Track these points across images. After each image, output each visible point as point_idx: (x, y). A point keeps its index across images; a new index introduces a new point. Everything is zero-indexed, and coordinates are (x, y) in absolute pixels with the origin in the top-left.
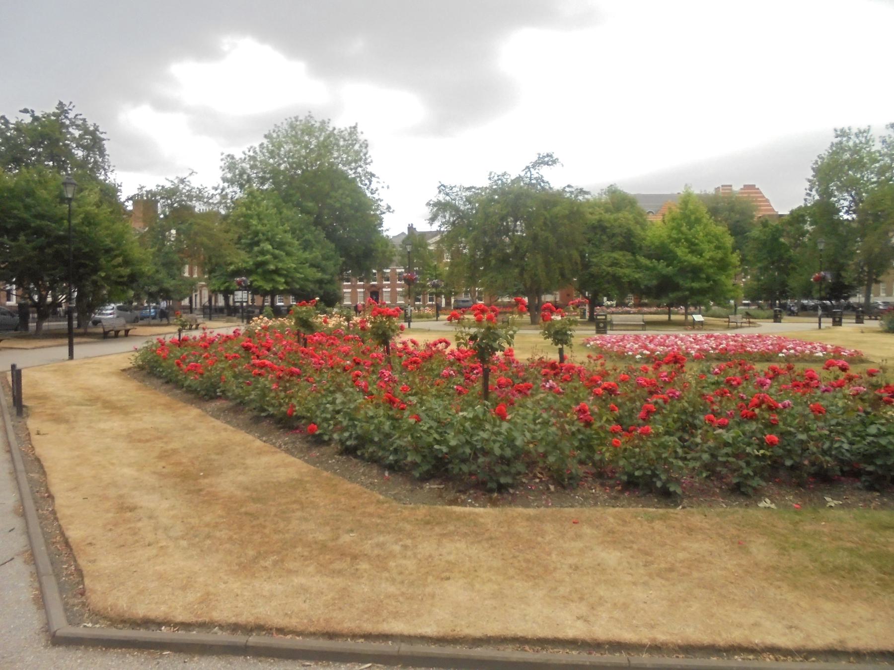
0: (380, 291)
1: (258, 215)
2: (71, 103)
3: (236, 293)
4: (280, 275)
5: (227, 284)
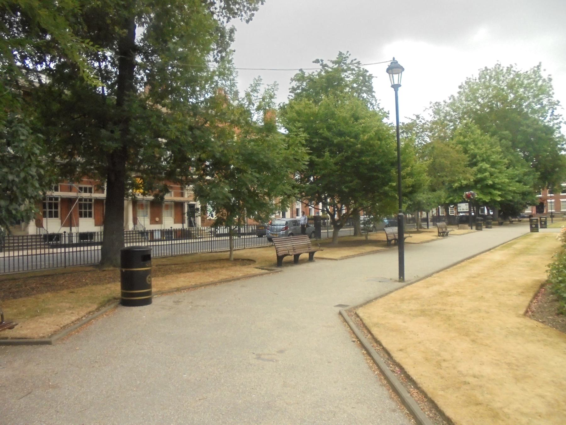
0: (545, 202)
1: (474, 141)
2: (348, 52)
3: (459, 205)
4: (495, 189)
5: (451, 198)
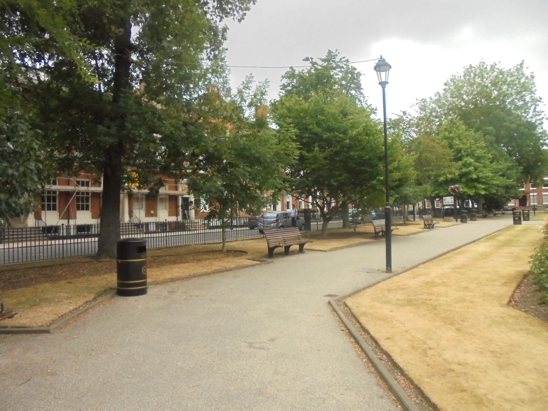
0: (528, 195)
1: (459, 137)
2: (337, 50)
3: (444, 198)
4: (480, 183)
5: (437, 192)
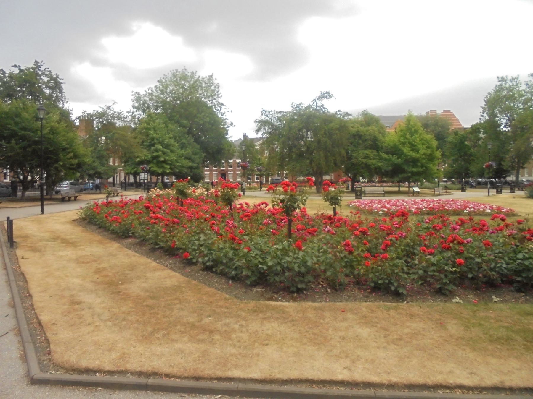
0: (227, 173)
1: (154, 128)
2: (42, 61)
3: (141, 174)
4: (167, 164)
5: (135, 169)
